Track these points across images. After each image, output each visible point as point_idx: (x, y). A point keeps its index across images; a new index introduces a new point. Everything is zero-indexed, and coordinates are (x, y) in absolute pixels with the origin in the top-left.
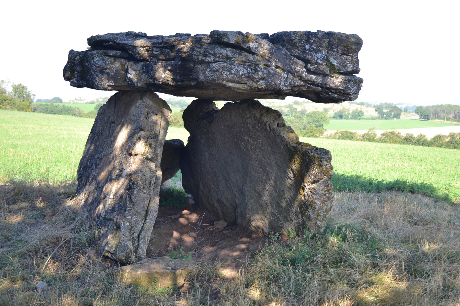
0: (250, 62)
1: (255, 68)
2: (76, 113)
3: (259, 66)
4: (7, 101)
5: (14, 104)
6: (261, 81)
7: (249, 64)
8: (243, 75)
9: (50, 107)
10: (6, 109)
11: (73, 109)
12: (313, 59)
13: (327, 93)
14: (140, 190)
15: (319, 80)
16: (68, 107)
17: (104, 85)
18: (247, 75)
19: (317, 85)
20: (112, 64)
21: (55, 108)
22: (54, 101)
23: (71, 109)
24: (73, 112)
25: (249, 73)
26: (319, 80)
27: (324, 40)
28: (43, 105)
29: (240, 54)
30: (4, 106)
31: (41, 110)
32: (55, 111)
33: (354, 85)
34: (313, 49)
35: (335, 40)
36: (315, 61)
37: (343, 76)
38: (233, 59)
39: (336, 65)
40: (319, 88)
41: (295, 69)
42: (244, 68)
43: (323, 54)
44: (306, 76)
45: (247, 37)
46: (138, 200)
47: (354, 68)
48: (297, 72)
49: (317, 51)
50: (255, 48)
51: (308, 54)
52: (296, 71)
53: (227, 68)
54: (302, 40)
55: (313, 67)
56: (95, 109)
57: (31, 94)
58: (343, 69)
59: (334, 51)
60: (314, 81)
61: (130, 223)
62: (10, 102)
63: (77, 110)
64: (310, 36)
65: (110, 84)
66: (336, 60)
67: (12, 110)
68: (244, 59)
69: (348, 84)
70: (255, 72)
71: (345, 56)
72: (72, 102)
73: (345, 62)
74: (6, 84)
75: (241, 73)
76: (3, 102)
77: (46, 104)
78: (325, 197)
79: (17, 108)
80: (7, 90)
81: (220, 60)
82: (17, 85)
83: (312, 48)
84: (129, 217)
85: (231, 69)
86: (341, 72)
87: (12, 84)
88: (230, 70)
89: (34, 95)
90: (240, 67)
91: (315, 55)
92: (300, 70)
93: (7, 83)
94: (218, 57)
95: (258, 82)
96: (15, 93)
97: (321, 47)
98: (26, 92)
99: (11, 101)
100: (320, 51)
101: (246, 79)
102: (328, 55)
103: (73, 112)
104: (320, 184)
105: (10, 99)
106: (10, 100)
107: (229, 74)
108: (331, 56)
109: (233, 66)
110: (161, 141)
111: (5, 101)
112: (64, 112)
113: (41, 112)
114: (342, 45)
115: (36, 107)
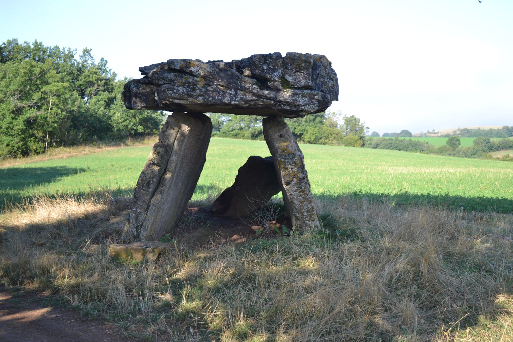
0: (189, 82)
1: (193, 87)
2: (425, 148)
3: (197, 86)
4: (333, 135)
5: (341, 138)
6: (200, 98)
8: (183, 93)
9: (394, 141)
10: (332, 144)
11: (421, 144)
12: (272, 77)
13: (279, 105)
14: (140, 187)
15: (272, 94)
16: (415, 141)
17: (138, 106)
18: (186, 93)
19: (270, 99)
20: (144, 89)
21: (400, 143)
22: (403, 134)
23: (419, 144)
24: (420, 147)
25: (188, 92)
26: (272, 94)
27: (278, 60)
28: (386, 140)
29: (182, 77)
30: (330, 142)
31: (384, 145)
32: (399, 146)
33: (303, 98)
34: (271, 68)
35: (287, 59)
37: (292, 91)
39: (291, 81)
40: (272, 101)
41: (244, 87)
42: (184, 87)
44: (258, 92)
45: (189, 63)
46: (139, 196)
48: (248, 89)
49: (274, 70)
50: (196, 72)
51: (266, 73)
52: (246, 88)
53: (170, 88)
54: (261, 62)
56: (447, 143)
57: (365, 127)
58: (298, 84)
59: (288, 69)
60: (266, 96)
61: (136, 214)
62: (336, 136)
63: (425, 145)
64: (267, 58)
66: (290, 77)
67: (339, 146)
68: (184, 81)
69: (296, 97)
70: (193, 91)
72: (424, 136)
74: (337, 116)
75: (181, 92)
76: (329, 137)
77: (389, 139)
78: (301, 198)
79: (344, 143)
80: (339, 122)
81: (167, 83)
82: (349, 117)
83: (269, 68)
84: (134, 209)
85: (174, 89)
86: (296, 86)
87: (344, 116)
88: (172, 90)
89: (368, 128)
90: (180, 87)
92: (250, 87)
93: (338, 115)
94: (166, 80)
95: (196, 98)
96: (347, 126)
97: (277, 67)
98: (359, 125)
99: (338, 136)
100: (277, 70)
101: (187, 96)
102: (284, 73)
103: (420, 147)
104: (293, 185)
105: (336, 133)
106: (337, 135)
108: (287, 73)
109: (175, 87)
110: (176, 150)
111: (332, 135)
112: (410, 147)
113: (384, 148)
114: (295, 63)
115: (379, 142)
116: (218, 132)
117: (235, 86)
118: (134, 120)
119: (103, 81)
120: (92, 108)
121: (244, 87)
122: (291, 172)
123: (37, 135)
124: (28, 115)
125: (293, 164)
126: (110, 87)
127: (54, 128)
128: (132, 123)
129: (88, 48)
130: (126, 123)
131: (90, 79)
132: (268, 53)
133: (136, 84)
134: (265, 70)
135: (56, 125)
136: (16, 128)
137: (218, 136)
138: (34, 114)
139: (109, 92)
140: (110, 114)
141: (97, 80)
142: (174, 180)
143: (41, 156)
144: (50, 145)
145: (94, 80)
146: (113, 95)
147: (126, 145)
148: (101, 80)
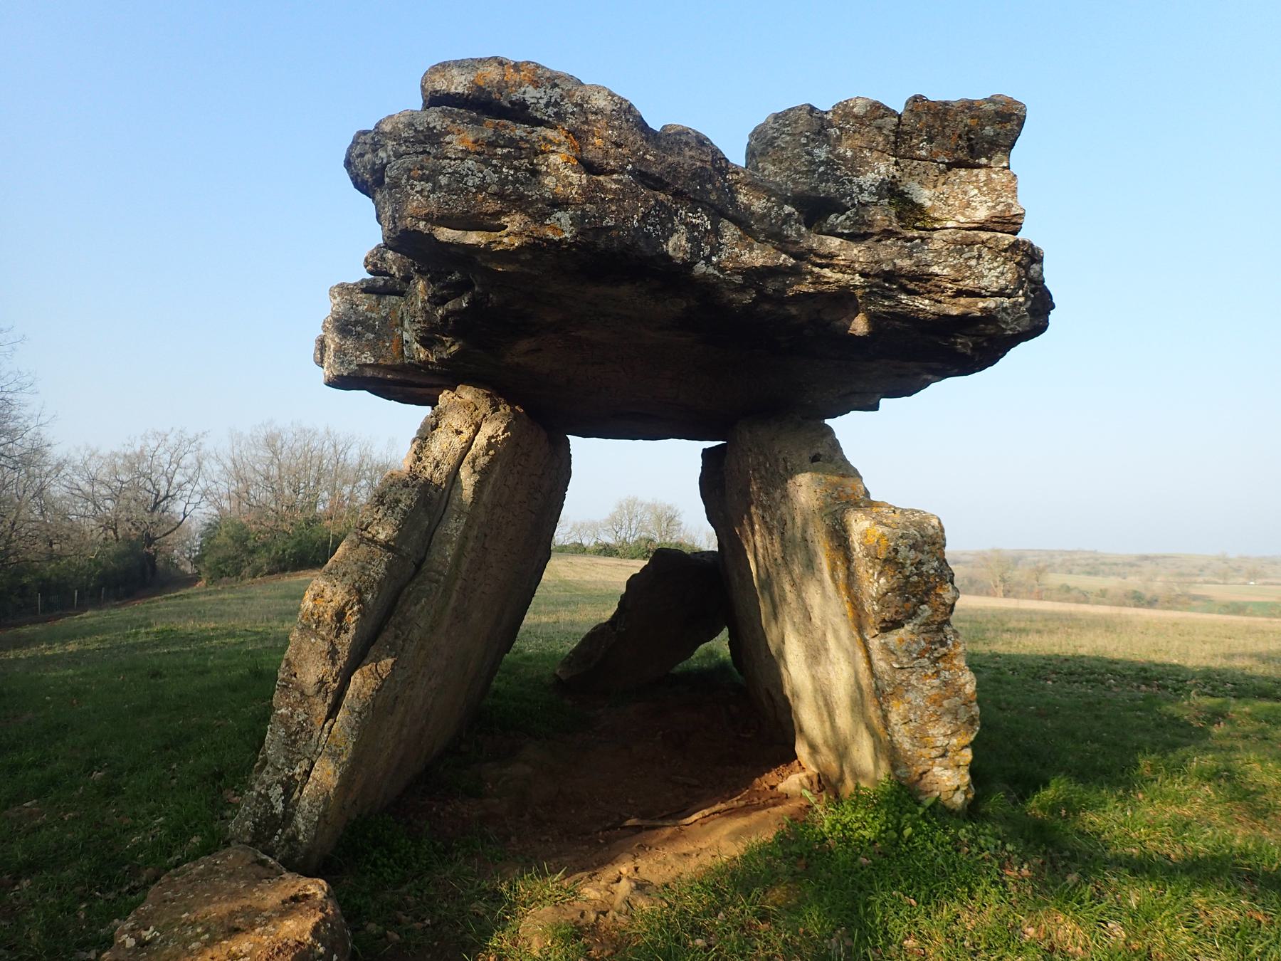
7: (506, 151)
8: (481, 188)
18: (493, 188)
25: (503, 182)
33: (995, 259)
36: (852, 199)
38: (447, 139)
40: (857, 277)
42: (486, 163)
43: (879, 173)
47: (1000, 208)
50: (547, 105)
55: (844, 217)
61: (288, 728)
65: (364, 360)
71: (963, 172)
73: (965, 193)
83: (838, 156)
90: (470, 163)
91: (850, 181)
107: (433, 191)
121: (747, 207)
122: (915, 578)
133: (350, 294)
134: (822, 163)
142: (452, 602)
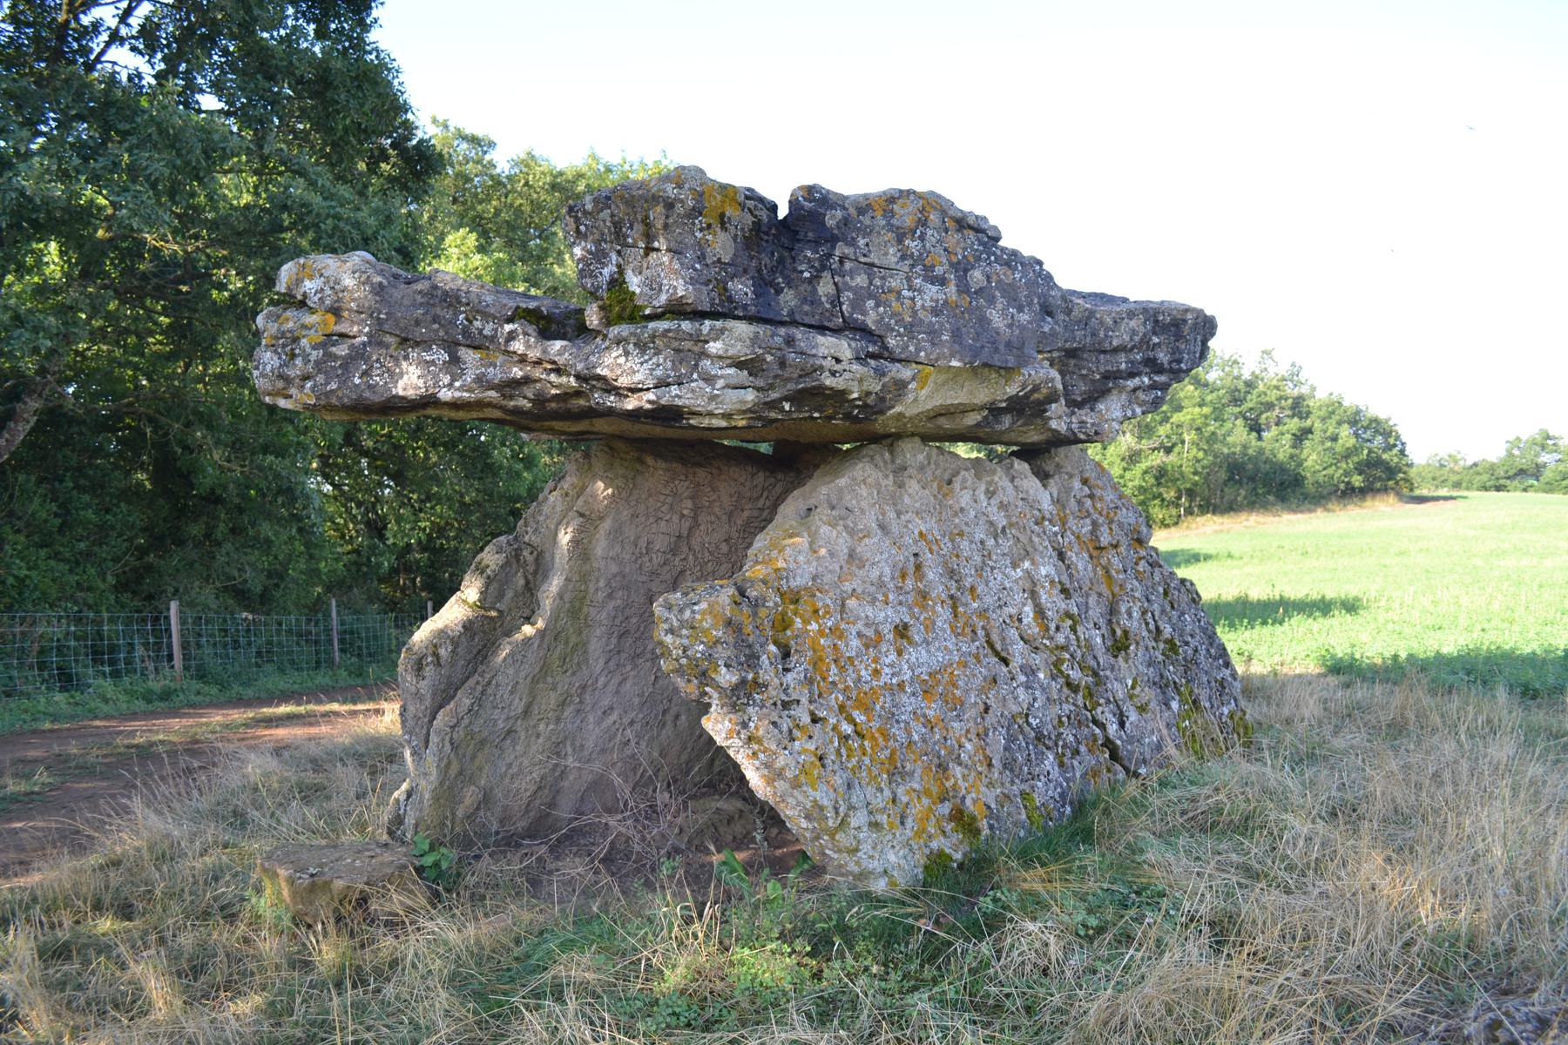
39: (638, 291)
86: (647, 312)
116: (1535, 483)
117: (441, 333)
118: (1344, 465)
119: (1290, 401)
120: (1269, 447)
123: (1165, 496)
124: (1149, 464)
125: (684, 632)
126: (1305, 410)
127: (1195, 484)
128: (1341, 471)
129: (1269, 348)
130: (1330, 471)
131: (1268, 399)
132: (1026, 251)
135: (1197, 478)
136: (1130, 484)
137: (1536, 491)
138: (1159, 461)
139: (1301, 418)
140: (1303, 457)
141: (1280, 399)
143: (1173, 529)
144: (1189, 512)
145: (1273, 399)
146: (1309, 422)
147: (1328, 510)
148: (1286, 399)
